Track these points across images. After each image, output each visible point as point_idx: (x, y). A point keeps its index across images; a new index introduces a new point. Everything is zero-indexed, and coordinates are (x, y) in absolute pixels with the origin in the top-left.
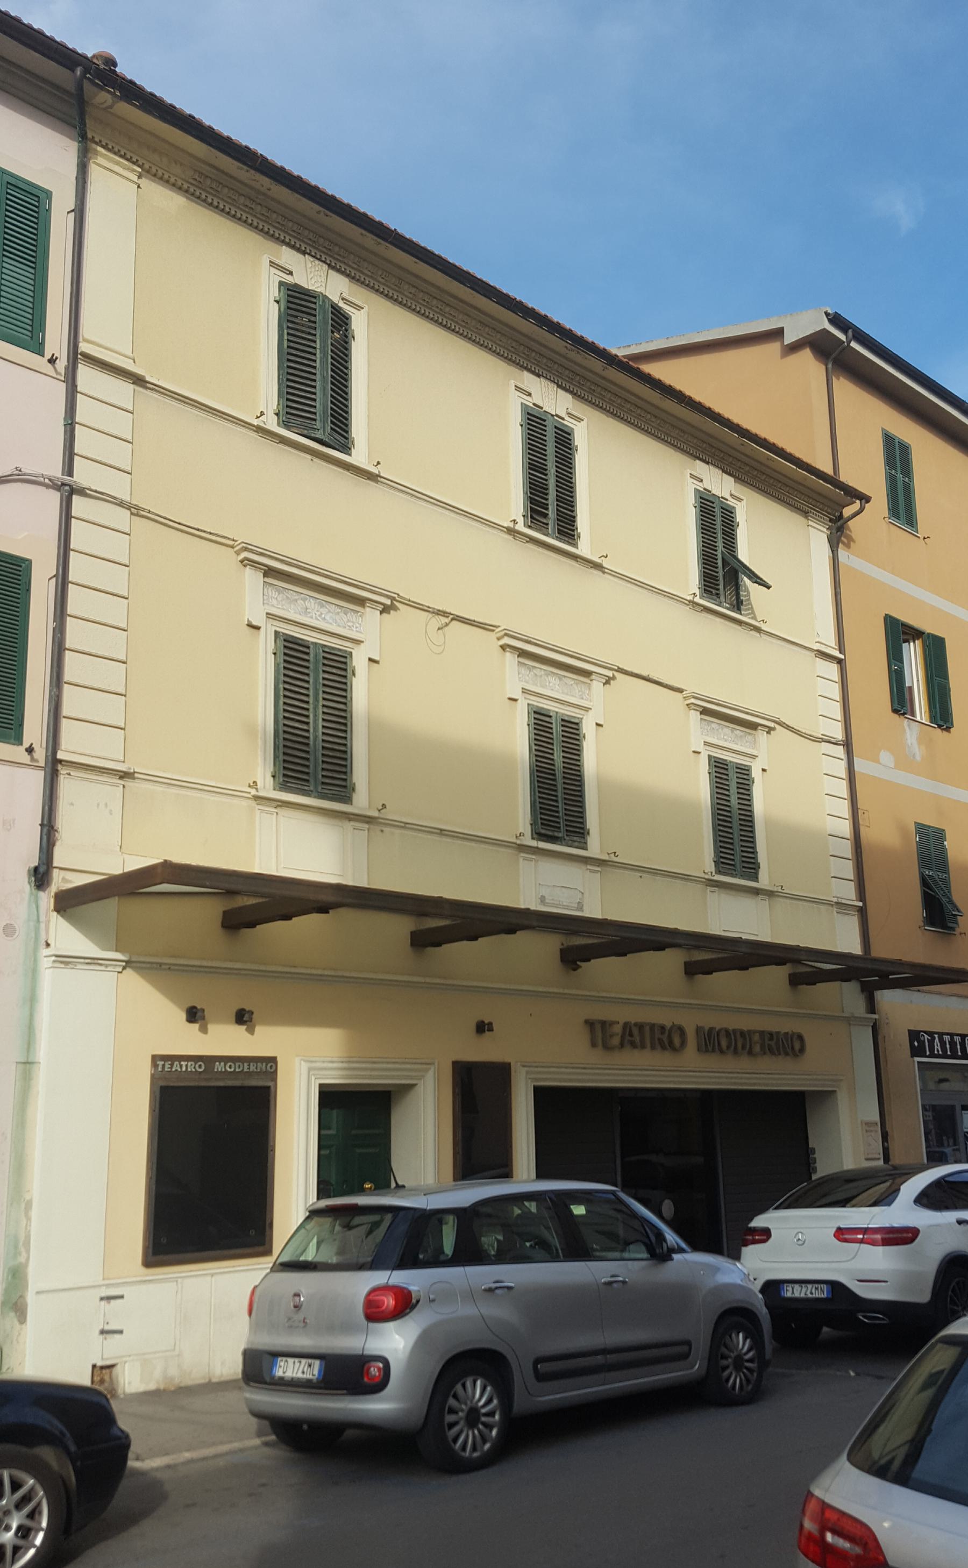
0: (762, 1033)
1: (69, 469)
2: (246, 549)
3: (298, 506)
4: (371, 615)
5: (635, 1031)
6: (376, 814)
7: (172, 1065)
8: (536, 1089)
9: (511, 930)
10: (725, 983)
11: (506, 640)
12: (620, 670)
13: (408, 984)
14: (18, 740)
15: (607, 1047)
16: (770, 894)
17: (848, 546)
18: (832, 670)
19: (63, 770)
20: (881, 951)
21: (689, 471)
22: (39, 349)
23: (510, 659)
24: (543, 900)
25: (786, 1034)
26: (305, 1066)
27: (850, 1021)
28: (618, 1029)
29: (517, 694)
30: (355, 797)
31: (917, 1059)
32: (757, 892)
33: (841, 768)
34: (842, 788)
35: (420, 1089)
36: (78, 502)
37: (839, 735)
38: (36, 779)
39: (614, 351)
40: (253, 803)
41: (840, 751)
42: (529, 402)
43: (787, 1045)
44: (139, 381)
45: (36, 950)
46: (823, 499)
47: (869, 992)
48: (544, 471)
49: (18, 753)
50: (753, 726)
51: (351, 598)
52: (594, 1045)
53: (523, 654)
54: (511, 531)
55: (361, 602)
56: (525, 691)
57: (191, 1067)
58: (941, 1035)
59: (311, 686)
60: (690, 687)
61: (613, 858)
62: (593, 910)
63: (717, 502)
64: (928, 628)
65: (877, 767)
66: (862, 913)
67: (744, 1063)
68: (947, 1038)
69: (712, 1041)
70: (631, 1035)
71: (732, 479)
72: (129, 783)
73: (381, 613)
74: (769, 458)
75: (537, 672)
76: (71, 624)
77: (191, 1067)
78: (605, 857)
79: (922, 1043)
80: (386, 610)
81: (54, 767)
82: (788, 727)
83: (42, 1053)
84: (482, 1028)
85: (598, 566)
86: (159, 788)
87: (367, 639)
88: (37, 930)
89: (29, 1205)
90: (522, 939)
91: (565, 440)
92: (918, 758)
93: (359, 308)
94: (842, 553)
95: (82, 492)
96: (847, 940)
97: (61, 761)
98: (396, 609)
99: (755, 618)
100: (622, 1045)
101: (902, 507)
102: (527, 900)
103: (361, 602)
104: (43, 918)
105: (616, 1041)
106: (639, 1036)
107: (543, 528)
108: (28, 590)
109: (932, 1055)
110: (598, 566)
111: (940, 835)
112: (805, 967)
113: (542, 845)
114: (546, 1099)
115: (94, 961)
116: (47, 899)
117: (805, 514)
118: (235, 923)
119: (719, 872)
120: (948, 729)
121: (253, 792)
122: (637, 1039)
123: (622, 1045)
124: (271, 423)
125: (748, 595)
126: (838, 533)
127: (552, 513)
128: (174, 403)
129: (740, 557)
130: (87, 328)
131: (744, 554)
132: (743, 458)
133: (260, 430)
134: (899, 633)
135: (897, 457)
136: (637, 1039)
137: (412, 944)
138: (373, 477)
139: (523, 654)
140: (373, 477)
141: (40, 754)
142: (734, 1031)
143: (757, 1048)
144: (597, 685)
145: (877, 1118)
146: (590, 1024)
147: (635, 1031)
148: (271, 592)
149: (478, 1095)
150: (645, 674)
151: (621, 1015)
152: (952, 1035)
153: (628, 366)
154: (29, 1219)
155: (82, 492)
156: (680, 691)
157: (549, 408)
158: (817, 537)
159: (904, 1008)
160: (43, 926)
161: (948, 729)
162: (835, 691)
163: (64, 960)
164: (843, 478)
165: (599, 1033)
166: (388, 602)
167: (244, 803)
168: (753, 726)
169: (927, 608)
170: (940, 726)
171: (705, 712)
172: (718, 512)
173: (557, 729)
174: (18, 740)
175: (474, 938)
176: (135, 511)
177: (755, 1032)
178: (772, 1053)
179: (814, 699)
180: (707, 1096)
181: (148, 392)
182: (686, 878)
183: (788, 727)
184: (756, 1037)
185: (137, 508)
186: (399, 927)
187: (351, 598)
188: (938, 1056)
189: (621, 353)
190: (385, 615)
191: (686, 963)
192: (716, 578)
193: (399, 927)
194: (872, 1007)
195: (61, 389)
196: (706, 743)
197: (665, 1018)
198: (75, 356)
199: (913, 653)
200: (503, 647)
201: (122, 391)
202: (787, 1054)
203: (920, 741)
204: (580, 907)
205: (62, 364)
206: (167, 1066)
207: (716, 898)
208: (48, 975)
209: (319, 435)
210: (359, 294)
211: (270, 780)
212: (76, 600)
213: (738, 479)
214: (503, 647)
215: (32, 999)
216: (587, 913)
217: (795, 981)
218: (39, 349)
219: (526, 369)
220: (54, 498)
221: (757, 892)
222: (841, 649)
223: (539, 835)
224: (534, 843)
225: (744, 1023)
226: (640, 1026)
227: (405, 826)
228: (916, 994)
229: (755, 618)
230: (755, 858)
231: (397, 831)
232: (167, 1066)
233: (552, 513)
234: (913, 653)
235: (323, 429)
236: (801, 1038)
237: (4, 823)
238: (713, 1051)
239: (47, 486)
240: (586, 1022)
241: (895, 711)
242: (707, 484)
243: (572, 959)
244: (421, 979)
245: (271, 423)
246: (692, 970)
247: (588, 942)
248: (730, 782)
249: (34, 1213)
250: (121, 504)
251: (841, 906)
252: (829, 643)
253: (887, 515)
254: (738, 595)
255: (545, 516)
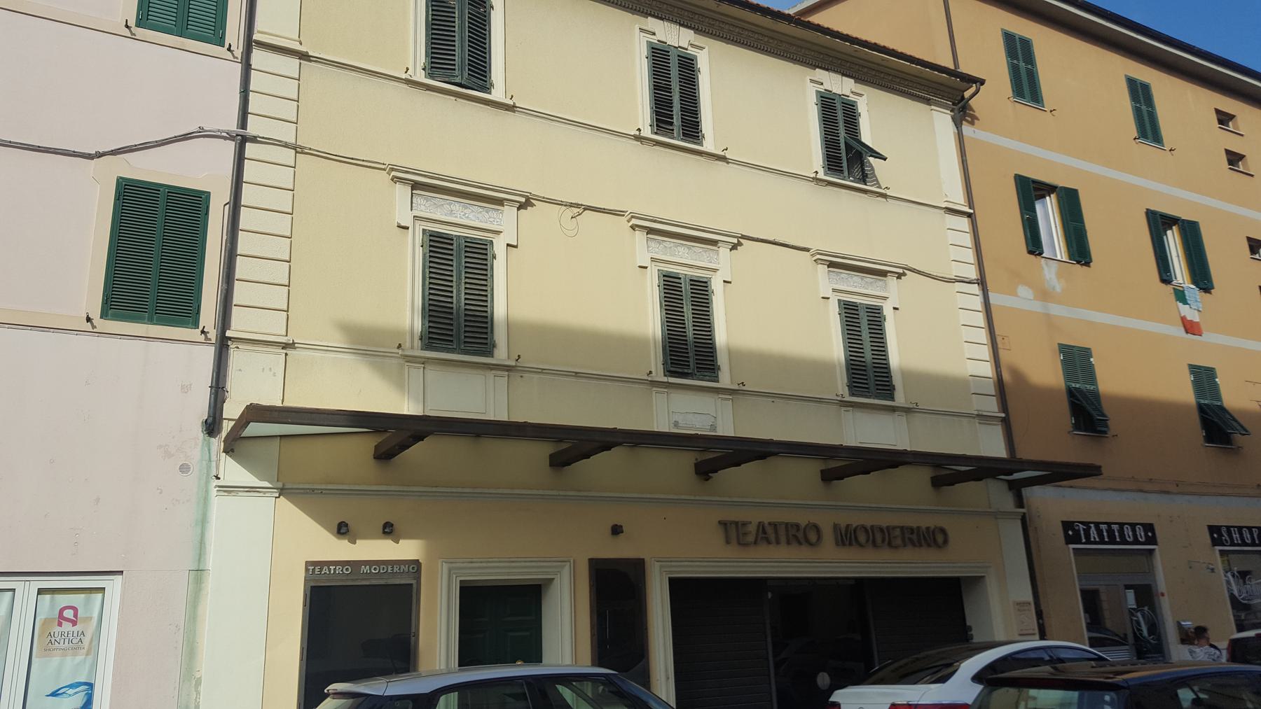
0: (902, 528)
1: (243, 123)
2: (393, 170)
3: (845, 221)
4: (892, 281)
5: (770, 530)
6: (513, 363)
7: (321, 570)
8: (670, 579)
9: (895, 465)
10: (858, 485)
11: (634, 221)
12: (744, 237)
13: (377, 493)
14: (196, 325)
15: (742, 544)
16: (907, 411)
17: (972, 123)
18: (964, 223)
19: (232, 345)
20: (1024, 453)
21: (808, 78)
22: (220, 41)
23: (640, 236)
24: (676, 424)
25: (928, 528)
26: (445, 566)
27: (997, 515)
28: (752, 529)
29: (829, 294)
30: (496, 352)
31: (1072, 546)
32: (893, 409)
33: (978, 303)
34: (980, 319)
35: (557, 583)
36: (250, 149)
37: (972, 273)
38: (208, 354)
39: (787, 12)
40: (401, 361)
41: (975, 289)
42: (654, 39)
43: (932, 538)
44: (304, 56)
45: (207, 483)
46: (949, 89)
47: (1016, 488)
48: (668, 90)
49: (195, 334)
50: (883, 274)
51: (491, 199)
52: (728, 542)
53: (651, 231)
54: (638, 138)
55: (500, 202)
56: (653, 260)
57: (339, 569)
58: (1097, 524)
59: (454, 268)
60: (814, 246)
61: (742, 388)
62: (726, 428)
63: (837, 98)
64: (1185, 216)
65: (1016, 300)
66: (1006, 423)
67: (886, 554)
68: (1104, 527)
69: (847, 537)
70: (764, 532)
71: (852, 81)
72: (290, 352)
73: (519, 209)
74: (883, 59)
75: (667, 244)
76: (241, 236)
77: (339, 569)
78: (736, 387)
79: (1077, 533)
80: (522, 206)
81: (223, 345)
82: (919, 272)
83: (211, 562)
84: (616, 530)
85: (723, 159)
86: (318, 354)
87: (720, 269)
88: (209, 467)
89: (198, 682)
90: (902, 471)
91: (688, 66)
92: (1058, 289)
93: (861, 95)
94: (966, 129)
95: (254, 139)
96: (992, 445)
97: (230, 338)
98: (533, 205)
99: (880, 187)
100: (755, 543)
101: (1026, 85)
102: (662, 425)
103: (500, 202)
104: (214, 458)
105: (751, 538)
106: (767, 534)
107: (669, 133)
108: (207, 213)
109: (1088, 542)
110: (723, 159)
111: (1086, 353)
112: (948, 471)
113: (672, 380)
114: (681, 589)
115: (251, 489)
116: (217, 443)
117: (928, 102)
118: (559, 462)
119: (852, 394)
120: (1087, 264)
121: (400, 352)
122: (772, 537)
123: (755, 543)
124: (421, 77)
125: (873, 169)
126: (962, 113)
127: (677, 120)
128: (335, 69)
129: (863, 140)
130: (259, 24)
131: (866, 137)
132: (717, 16)
133: (409, 82)
134: (1030, 191)
135: (1019, 50)
136: (772, 537)
137: (551, 465)
138: (511, 108)
139: (651, 231)
140: (511, 108)
141: (213, 335)
142: (872, 527)
143: (899, 541)
144: (724, 251)
145: (1030, 598)
146: (724, 524)
147: (770, 530)
148: (653, 244)
149: (615, 589)
150: (771, 239)
151: (755, 517)
152: (1109, 524)
153: (798, 20)
154: (198, 693)
155: (254, 139)
156: (807, 250)
157: (837, 90)
158: (942, 119)
159: (1055, 504)
160: (214, 464)
161: (1087, 264)
162: (967, 240)
163: (228, 490)
164: (963, 69)
165: (734, 532)
166: (523, 200)
167: (394, 361)
168: (883, 274)
169: (1178, 200)
170: (1078, 262)
171: (832, 265)
172: (839, 106)
173: (686, 288)
174: (196, 325)
175: (868, 473)
176: (298, 149)
177: (894, 528)
178: (914, 545)
179: (952, 248)
180: (860, 582)
181: (313, 64)
182: (820, 401)
183: (919, 272)
184: (898, 532)
185: (301, 147)
186: (541, 451)
187: (491, 199)
188: (1095, 543)
189: (792, 12)
190: (522, 211)
191: (822, 471)
192: (840, 158)
193: (541, 451)
194: (1020, 502)
195: (238, 68)
196: (834, 290)
197: (802, 519)
198: (250, 44)
199: (1173, 239)
200: (633, 227)
201: (290, 65)
202: (929, 545)
203: (1059, 275)
204: (713, 427)
205: (238, 53)
206: (317, 570)
207: (849, 416)
208: (217, 503)
209: (458, 80)
210: (860, 88)
211: (661, 367)
212: (247, 218)
213: (698, 31)
214: (633, 227)
215: (203, 521)
216: (720, 433)
217: (937, 483)
218: (220, 41)
219: (651, 15)
220: (230, 147)
221: (893, 409)
222: (971, 205)
223: (670, 373)
224: (665, 379)
225: (885, 521)
226: (775, 526)
227: (542, 371)
228: (1068, 492)
229: (880, 187)
230: (890, 381)
231: (536, 376)
232: (317, 570)
233: (677, 120)
234: (1173, 239)
235: (461, 74)
236: (943, 531)
237: (183, 387)
238: (850, 544)
239: (225, 138)
240: (720, 522)
241: (1031, 252)
242: (827, 86)
243: (705, 471)
244: (397, 488)
245: (421, 77)
246: (828, 477)
247: (717, 456)
248: (862, 323)
249: (202, 689)
250: (286, 145)
251: (983, 418)
252: (959, 201)
253: (1136, 135)
254: (863, 170)
255: (671, 124)
